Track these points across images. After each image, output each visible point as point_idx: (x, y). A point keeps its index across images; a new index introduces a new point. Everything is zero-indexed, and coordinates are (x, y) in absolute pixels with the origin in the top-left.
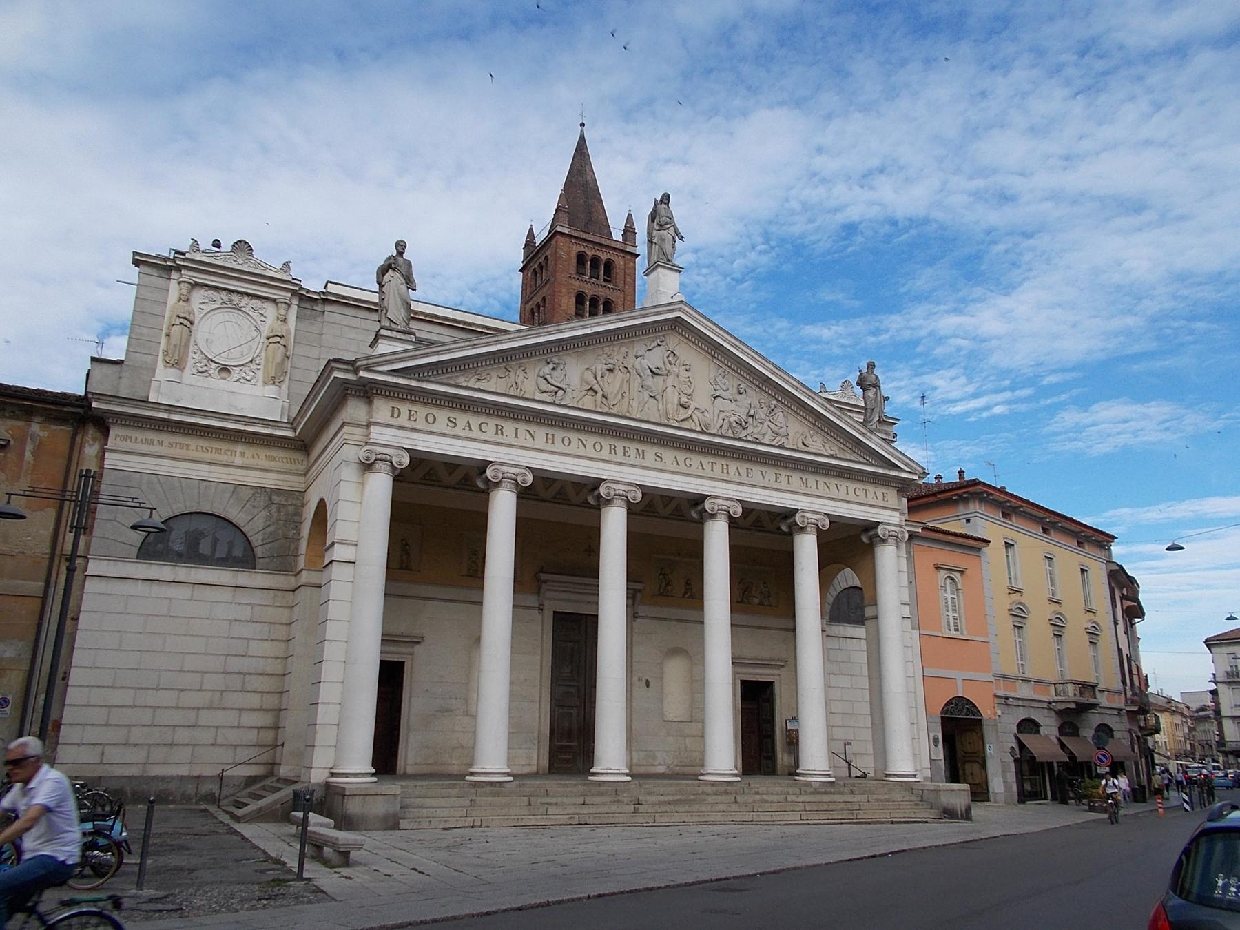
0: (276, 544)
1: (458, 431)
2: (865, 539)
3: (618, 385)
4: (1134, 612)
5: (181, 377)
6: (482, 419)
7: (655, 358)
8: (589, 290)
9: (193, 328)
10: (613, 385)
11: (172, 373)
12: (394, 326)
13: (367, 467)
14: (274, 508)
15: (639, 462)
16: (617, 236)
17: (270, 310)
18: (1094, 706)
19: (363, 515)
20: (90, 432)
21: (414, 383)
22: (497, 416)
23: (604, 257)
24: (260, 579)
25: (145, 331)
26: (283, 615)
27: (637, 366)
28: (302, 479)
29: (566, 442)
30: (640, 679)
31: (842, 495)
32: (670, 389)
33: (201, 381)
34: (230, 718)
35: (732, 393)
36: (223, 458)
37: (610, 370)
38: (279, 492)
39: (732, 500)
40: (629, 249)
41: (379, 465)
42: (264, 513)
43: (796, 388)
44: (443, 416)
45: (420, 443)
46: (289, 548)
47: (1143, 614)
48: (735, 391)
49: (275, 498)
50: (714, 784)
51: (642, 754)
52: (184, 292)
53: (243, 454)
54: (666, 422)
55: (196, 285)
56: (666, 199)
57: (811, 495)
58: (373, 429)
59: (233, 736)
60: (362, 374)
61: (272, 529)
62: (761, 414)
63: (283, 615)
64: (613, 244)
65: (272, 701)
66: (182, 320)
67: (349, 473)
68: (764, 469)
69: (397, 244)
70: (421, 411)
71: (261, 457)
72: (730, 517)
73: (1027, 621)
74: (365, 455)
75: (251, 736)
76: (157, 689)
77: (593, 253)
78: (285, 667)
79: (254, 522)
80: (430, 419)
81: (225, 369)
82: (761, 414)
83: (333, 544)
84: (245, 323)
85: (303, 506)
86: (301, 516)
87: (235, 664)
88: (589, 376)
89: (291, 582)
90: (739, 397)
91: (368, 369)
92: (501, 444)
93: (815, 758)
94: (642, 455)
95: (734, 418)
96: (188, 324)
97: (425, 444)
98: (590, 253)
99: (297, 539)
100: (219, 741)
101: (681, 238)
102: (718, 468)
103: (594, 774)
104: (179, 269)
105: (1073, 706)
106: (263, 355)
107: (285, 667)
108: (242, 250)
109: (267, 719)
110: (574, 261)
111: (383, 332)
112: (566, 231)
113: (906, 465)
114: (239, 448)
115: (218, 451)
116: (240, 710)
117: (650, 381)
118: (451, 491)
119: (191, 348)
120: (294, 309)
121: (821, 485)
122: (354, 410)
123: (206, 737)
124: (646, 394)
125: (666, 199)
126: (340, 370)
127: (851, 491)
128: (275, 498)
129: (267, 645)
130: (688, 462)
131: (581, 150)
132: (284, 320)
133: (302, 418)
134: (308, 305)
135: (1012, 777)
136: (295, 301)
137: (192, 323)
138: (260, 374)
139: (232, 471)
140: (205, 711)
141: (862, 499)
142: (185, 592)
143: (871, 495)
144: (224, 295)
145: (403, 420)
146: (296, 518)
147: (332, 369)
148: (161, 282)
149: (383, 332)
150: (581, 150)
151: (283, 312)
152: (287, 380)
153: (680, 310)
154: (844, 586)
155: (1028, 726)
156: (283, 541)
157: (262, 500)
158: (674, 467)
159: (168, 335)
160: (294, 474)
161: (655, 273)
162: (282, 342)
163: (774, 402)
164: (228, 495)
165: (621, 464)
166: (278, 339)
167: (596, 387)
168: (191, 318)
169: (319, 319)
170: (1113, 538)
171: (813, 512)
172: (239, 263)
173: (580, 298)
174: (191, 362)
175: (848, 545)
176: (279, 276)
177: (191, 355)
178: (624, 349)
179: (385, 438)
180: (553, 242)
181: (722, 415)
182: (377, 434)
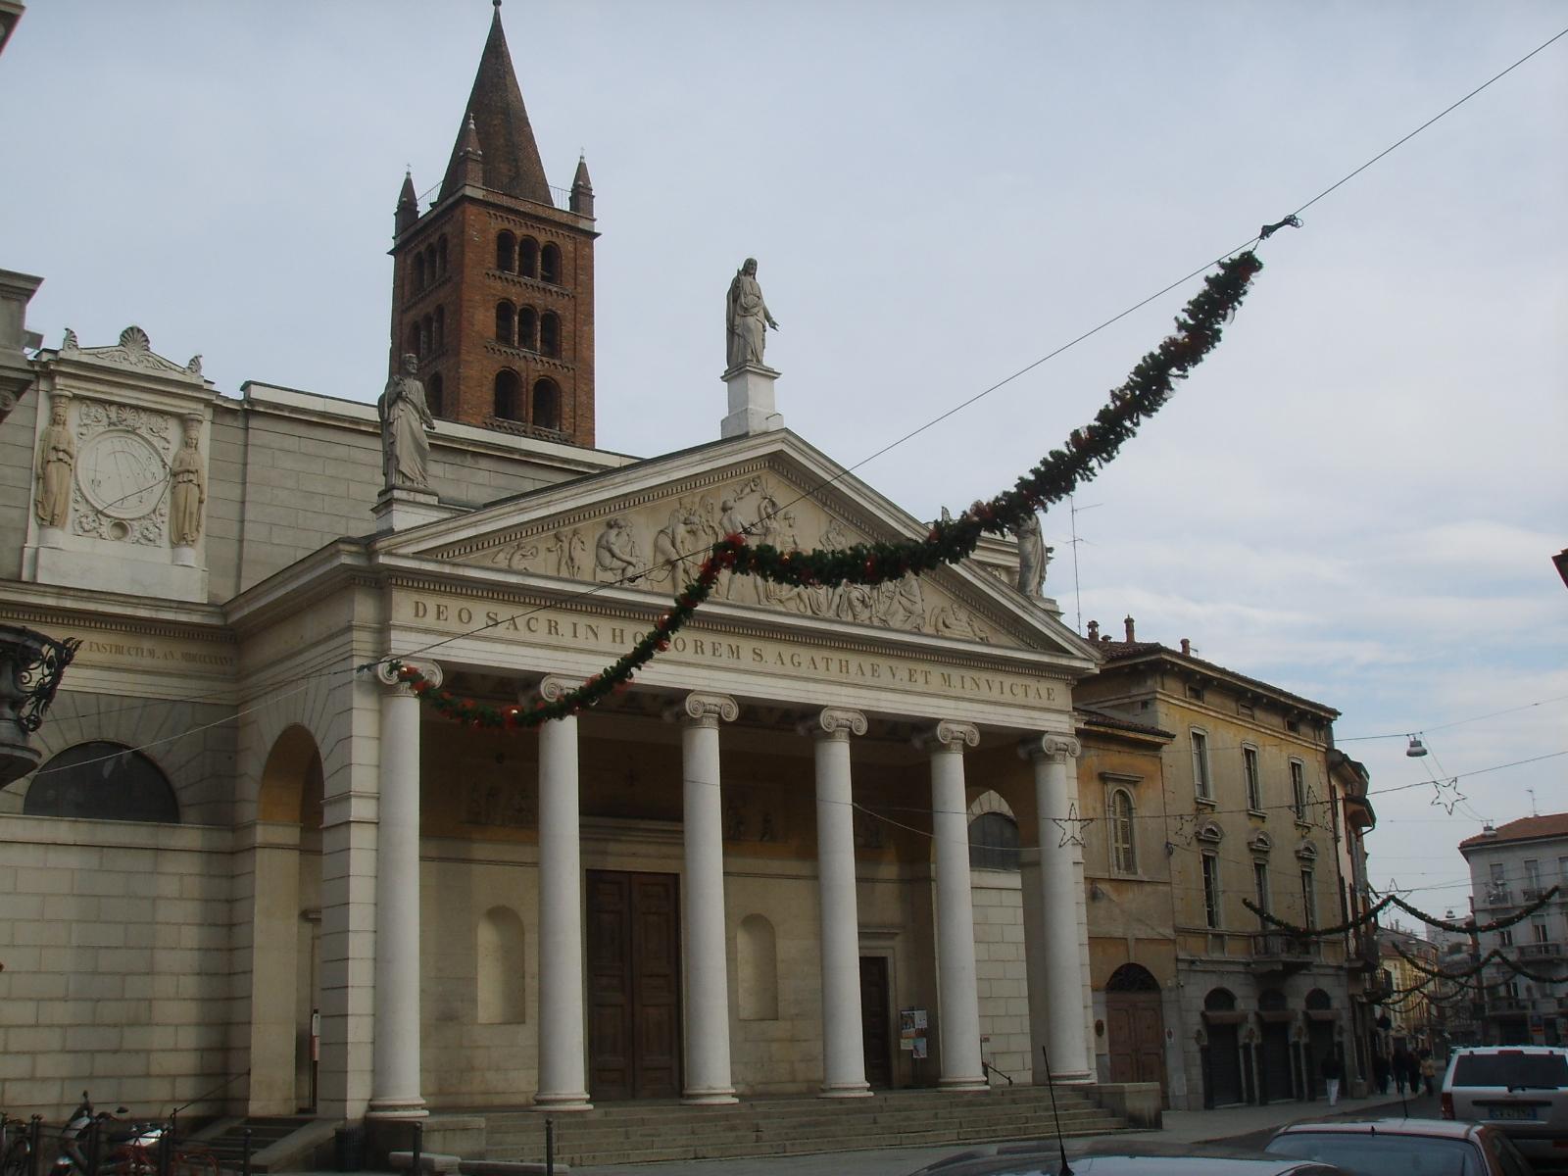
2: (1022, 753)
4: (1361, 816)
8: (519, 296)
12: (408, 484)
13: (384, 692)
15: (733, 663)
16: (561, 201)
18: (1306, 966)
19: (383, 759)
21: (447, 569)
23: (542, 238)
24: (189, 836)
31: (995, 695)
33: (84, 544)
39: (854, 711)
40: (583, 225)
44: (481, 611)
47: (1373, 820)
50: (841, 1100)
54: (765, 604)
56: (750, 268)
57: (957, 698)
64: (557, 218)
68: (894, 663)
70: (454, 605)
73: (1220, 846)
77: (524, 231)
80: (465, 616)
81: (121, 526)
84: (135, 446)
92: (556, 648)
93: (716, 1067)
94: (735, 652)
96: (66, 458)
98: (520, 232)
101: (773, 325)
102: (834, 666)
104: (50, 375)
108: (135, 341)
110: (493, 247)
112: (479, 194)
113: (1080, 649)
119: (72, 495)
121: (968, 683)
125: (750, 268)
127: (1006, 689)
131: (496, 51)
135: (1197, 1072)
136: (208, 414)
141: (1020, 699)
143: (1032, 693)
144: (113, 411)
145: (430, 620)
147: (338, 552)
150: (496, 51)
154: (986, 809)
155: (1220, 998)
158: (778, 669)
165: (709, 667)
171: (959, 722)
172: (133, 363)
173: (504, 309)
174: (71, 515)
175: (1006, 761)
176: (187, 379)
180: (458, 212)
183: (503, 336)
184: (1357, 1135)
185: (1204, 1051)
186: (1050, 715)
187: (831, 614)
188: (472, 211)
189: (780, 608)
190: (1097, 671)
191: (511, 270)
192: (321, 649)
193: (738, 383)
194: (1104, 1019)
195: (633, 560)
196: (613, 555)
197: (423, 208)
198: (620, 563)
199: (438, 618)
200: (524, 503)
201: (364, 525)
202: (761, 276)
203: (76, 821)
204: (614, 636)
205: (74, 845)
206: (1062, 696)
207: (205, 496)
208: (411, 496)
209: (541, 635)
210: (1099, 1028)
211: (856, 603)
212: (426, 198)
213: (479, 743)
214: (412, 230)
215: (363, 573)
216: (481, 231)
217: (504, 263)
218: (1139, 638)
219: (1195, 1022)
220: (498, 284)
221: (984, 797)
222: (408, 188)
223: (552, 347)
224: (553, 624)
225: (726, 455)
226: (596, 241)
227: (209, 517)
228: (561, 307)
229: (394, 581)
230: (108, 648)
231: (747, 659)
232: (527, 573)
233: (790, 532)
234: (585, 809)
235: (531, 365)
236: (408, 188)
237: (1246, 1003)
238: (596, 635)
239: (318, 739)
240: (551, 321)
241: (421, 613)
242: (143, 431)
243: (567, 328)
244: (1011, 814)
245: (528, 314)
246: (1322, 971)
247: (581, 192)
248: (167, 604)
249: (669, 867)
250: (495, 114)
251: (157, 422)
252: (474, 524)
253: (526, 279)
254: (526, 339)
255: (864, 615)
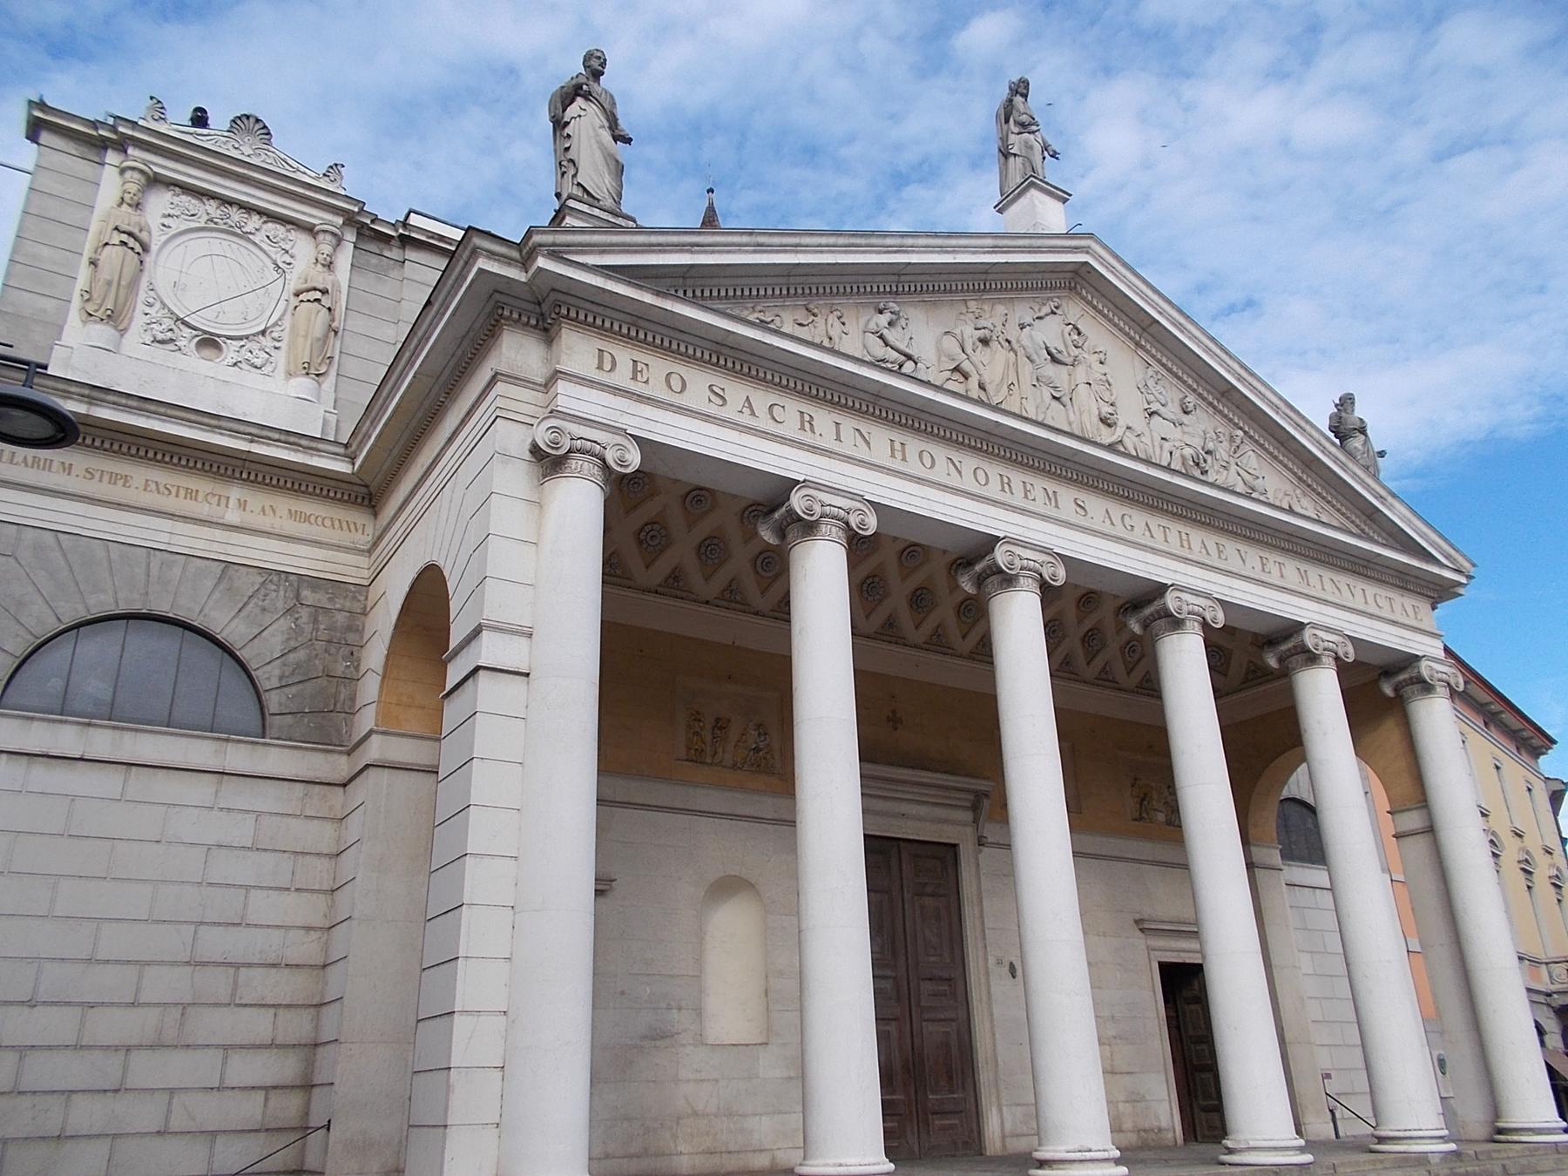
0: (309, 687)
1: (728, 412)
3: (1000, 369)
5: (118, 345)
6: (774, 397)
7: (1050, 332)
9: (148, 259)
10: (992, 366)
11: (101, 333)
13: (549, 462)
14: (304, 614)
17: (303, 246)
19: (535, 572)
21: (648, 298)
22: (801, 393)
25: (45, 251)
26: (322, 836)
27: (1025, 342)
28: (363, 561)
29: (928, 462)
30: (999, 962)
32: (1083, 388)
34: (204, 1068)
35: (1173, 411)
36: (202, 509)
37: (985, 342)
38: (316, 583)
41: (576, 463)
42: (285, 624)
43: (1277, 409)
45: (658, 428)
46: (336, 696)
48: (1179, 410)
49: (308, 595)
51: (1019, 1111)
52: (133, 188)
53: (242, 505)
55: (155, 181)
58: (562, 386)
59: (211, 1111)
60: (541, 262)
61: (301, 655)
62: (1223, 451)
63: (322, 836)
65: (297, 1026)
66: (124, 237)
67: (515, 477)
69: (588, 57)
71: (277, 510)
72: (1205, 625)
74: (549, 436)
75: (250, 1109)
76: (31, 1004)
78: (326, 948)
79: (266, 643)
81: (209, 342)
82: (1223, 451)
83: (477, 632)
85: (365, 613)
86: (360, 631)
87: (217, 943)
88: (950, 345)
89: (341, 766)
90: (1186, 419)
91: (556, 254)
95: (1188, 452)
96: (138, 248)
99: (352, 680)
100: (175, 1125)
103: (1230, 1151)
104: (121, 145)
106: (287, 323)
107: (326, 948)
108: (250, 132)
109: (285, 1068)
111: (571, 203)
113: (1447, 557)
114: (236, 492)
115: (192, 494)
117: (1050, 370)
118: (651, 597)
120: (348, 249)
122: (516, 351)
123: (145, 1115)
124: (1046, 393)
126: (492, 255)
128: (308, 595)
129: (290, 899)
130: (1127, 521)
132: (329, 266)
133: (374, 423)
134: (373, 247)
136: (350, 236)
137: (145, 248)
138: (280, 358)
139: (218, 534)
140: (145, 1054)
142: (110, 782)
144: (212, 207)
145: (621, 377)
146: (351, 637)
147: (475, 253)
148: (84, 168)
149: (571, 203)
151: (327, 249)
152: (333, 372)
153: (1086, 250)
156: (323, 682)
157: (280, 599)
159: (93, 263)
160: (347, 549)
161: (1023, 201)
162: (326, 301)
163: (1240, 433)
164: (210, 583)
166: (318, 295)
167: (966, 366)
168: (144, 236)
169: (394, 274)
171: (1328, 630)
172: (245, 149)
174: (139, 321)
177: (140, 307)
178: (1000, 309)
181: (1167, 445)
182: (569, 396)
184: (1272, 1144)
198: (896, 354)
199: (634, 378)
203: (89, 725)
204: (893, 450)
205: (81, 759)
209: (791, 428)
224: (807, 418)
229: (564, 311)
230: (174, 491)
231: (1067, 510)
233: (1103, 369)
238: (868, 443)
241: (607, 366)
248: (276, 436)
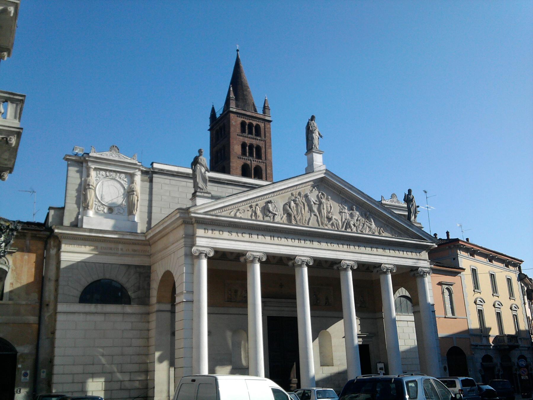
8: (248, 141)
12: (201, 191)
16: (260, 111)
20: (52, 243)
23: (254, 123)
39: (353, 261)
40: (267, 118)
45: (217, 244)
54: (321, 226)
56: (313, 118)
79: (128, 282)
97: (220, 244)
98: (247, 121)
100: (122, 387)
105: (507, 347)
112: (234, 110)
116: (130, 372)
170: (522, 261)
173: (244, 145)
174: (94, 206)
175: (408, 278)
179: (203, 243)
183: (244, 153)
185: (482, 376)
186: (422, 261)
187: (343, 229)
188: (232, 115)
189: (326, 228)
190: (437, 246)
191: (245, 133)
192: (176, 244)
193: (310, 156)
194: (447, 366)
195: (277, 213)
196: (270, 212)
197: (218, 116)
200: (239, 195)
201: (189, 204)
202: (315, 123)
206: (425, 255)
207: (139, 199)
208: (202, 194)
210: (445, 369)
211: (352, 225)
212: (219, 112)
213: (228, 272)
214: (215, 122)
215: (188, 222)
216: (235, 122)
217: (243, 130)
218: (451, 237)
219: (478, 365)
220: (241, 138)
221: (400, 290)
222: (213, 110)
223: (259, 156)
225: (307, 178)
226: (271, 123)
227: (141, 205)
228: (261, 144)
232: (241, 218)
234: (263, 297)
235: (254, 163)
236: (213, 110)
237: (497, 360)
239: (174, 275)
240: (258, 149)
242: (117, 178)
243: (263, 150)
244: (409, 296)
245: (251, 146)
246: (523, 349)
247: (265, 108)
249: (286, 313)
250: (237, 82)
251: (123, 176)
252: (223, 202)
253: (250, 136)
254: (251, 154)
255: (354, 229)
